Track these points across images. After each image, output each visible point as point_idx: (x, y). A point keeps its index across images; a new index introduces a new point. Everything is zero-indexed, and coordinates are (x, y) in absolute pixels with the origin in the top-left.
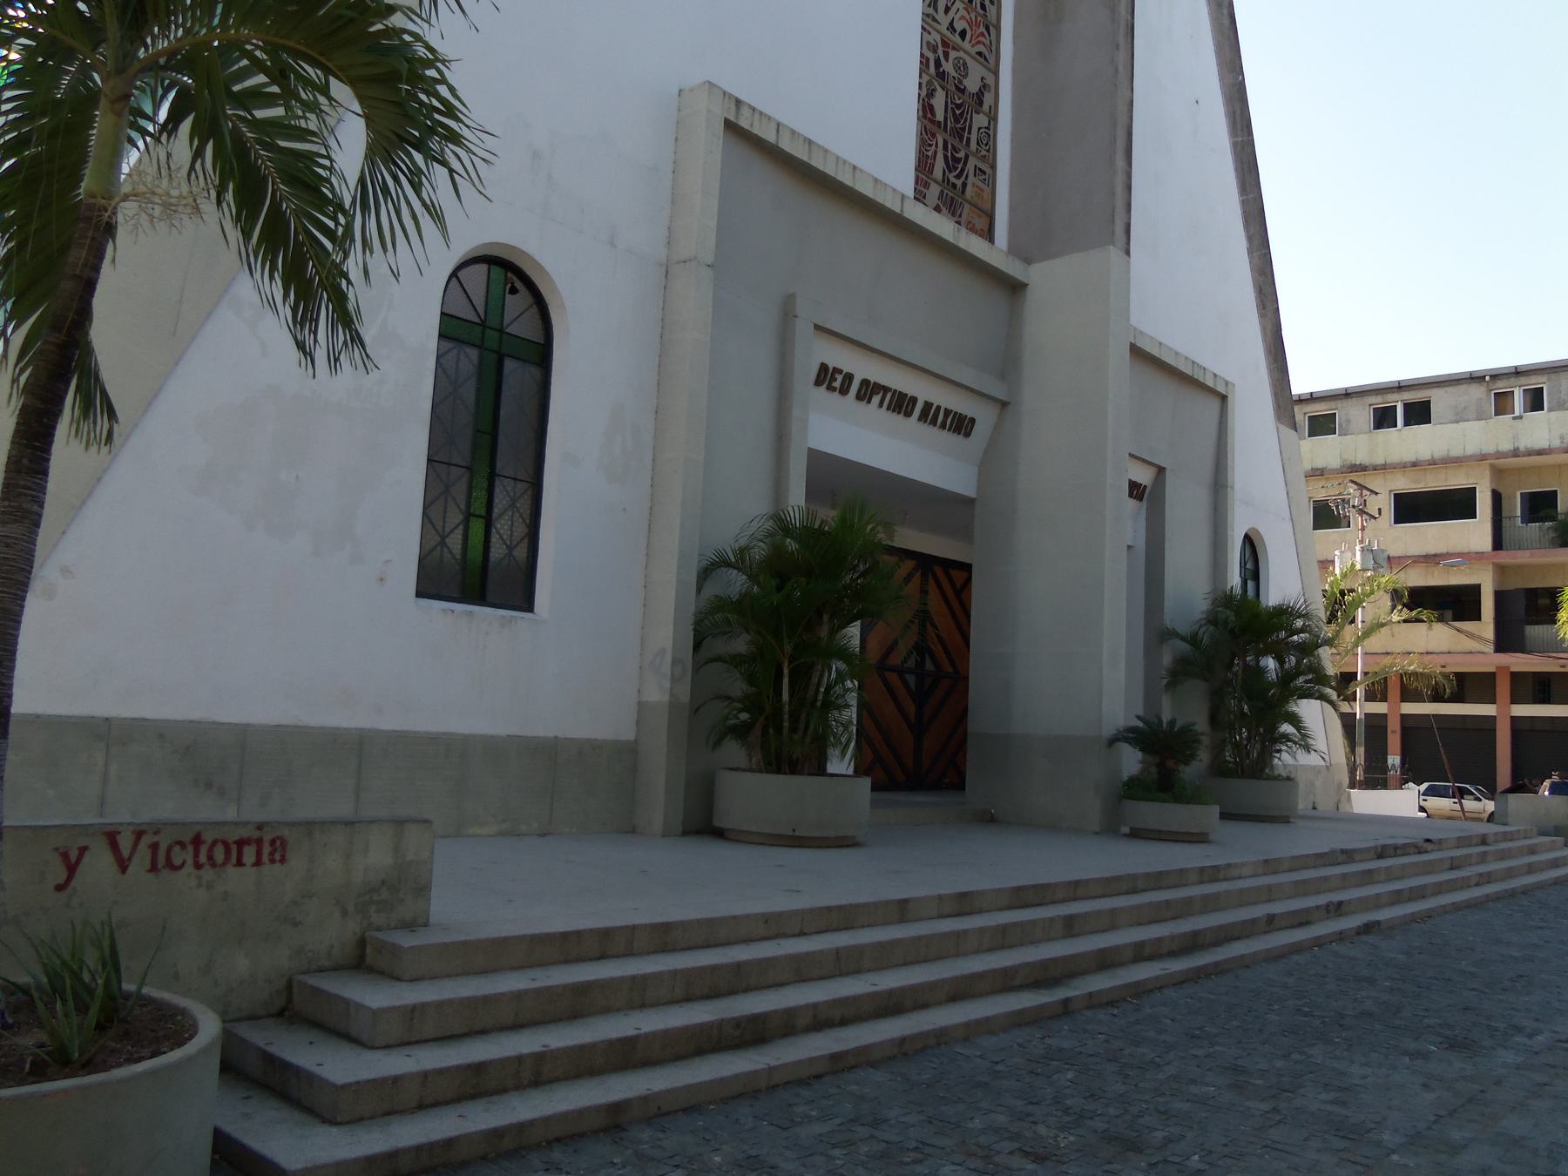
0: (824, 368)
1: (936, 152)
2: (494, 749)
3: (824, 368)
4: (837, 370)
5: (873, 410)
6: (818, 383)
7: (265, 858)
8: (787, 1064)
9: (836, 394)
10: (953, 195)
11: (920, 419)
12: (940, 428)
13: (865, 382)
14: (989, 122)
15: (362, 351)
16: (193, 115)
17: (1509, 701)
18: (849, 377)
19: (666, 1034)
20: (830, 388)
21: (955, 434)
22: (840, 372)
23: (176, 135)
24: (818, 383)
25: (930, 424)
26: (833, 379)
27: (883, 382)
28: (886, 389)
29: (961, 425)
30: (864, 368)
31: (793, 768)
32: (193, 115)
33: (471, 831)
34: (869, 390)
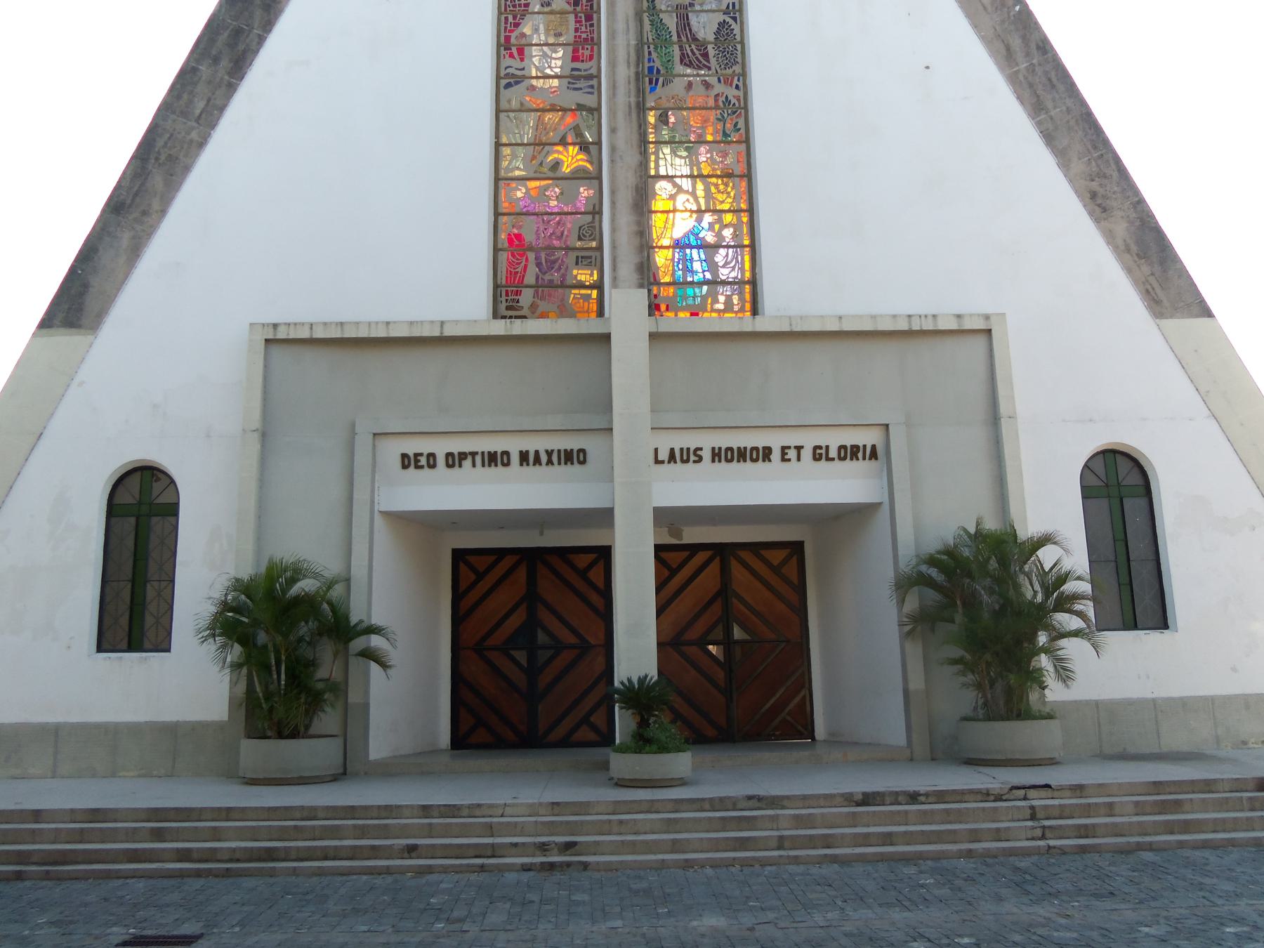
0: (404, 456)
1: (526, 267)
2: (135, 730)
3: (404, 456)
6: (405, 467)
8: (935, 590)
9: (426, 471)
10: (516, 289)
12: (870, 459)
14: (692, 267)
17: (693, 312)
19: (305, 847)
21: (493, 467)
22: (421, 455)
24: (405, 467)
25: (534, 465)
26: (417, 461)
27: (467, 449)
28: (474, 454)
31: (294, 735)
33: (121, 774)
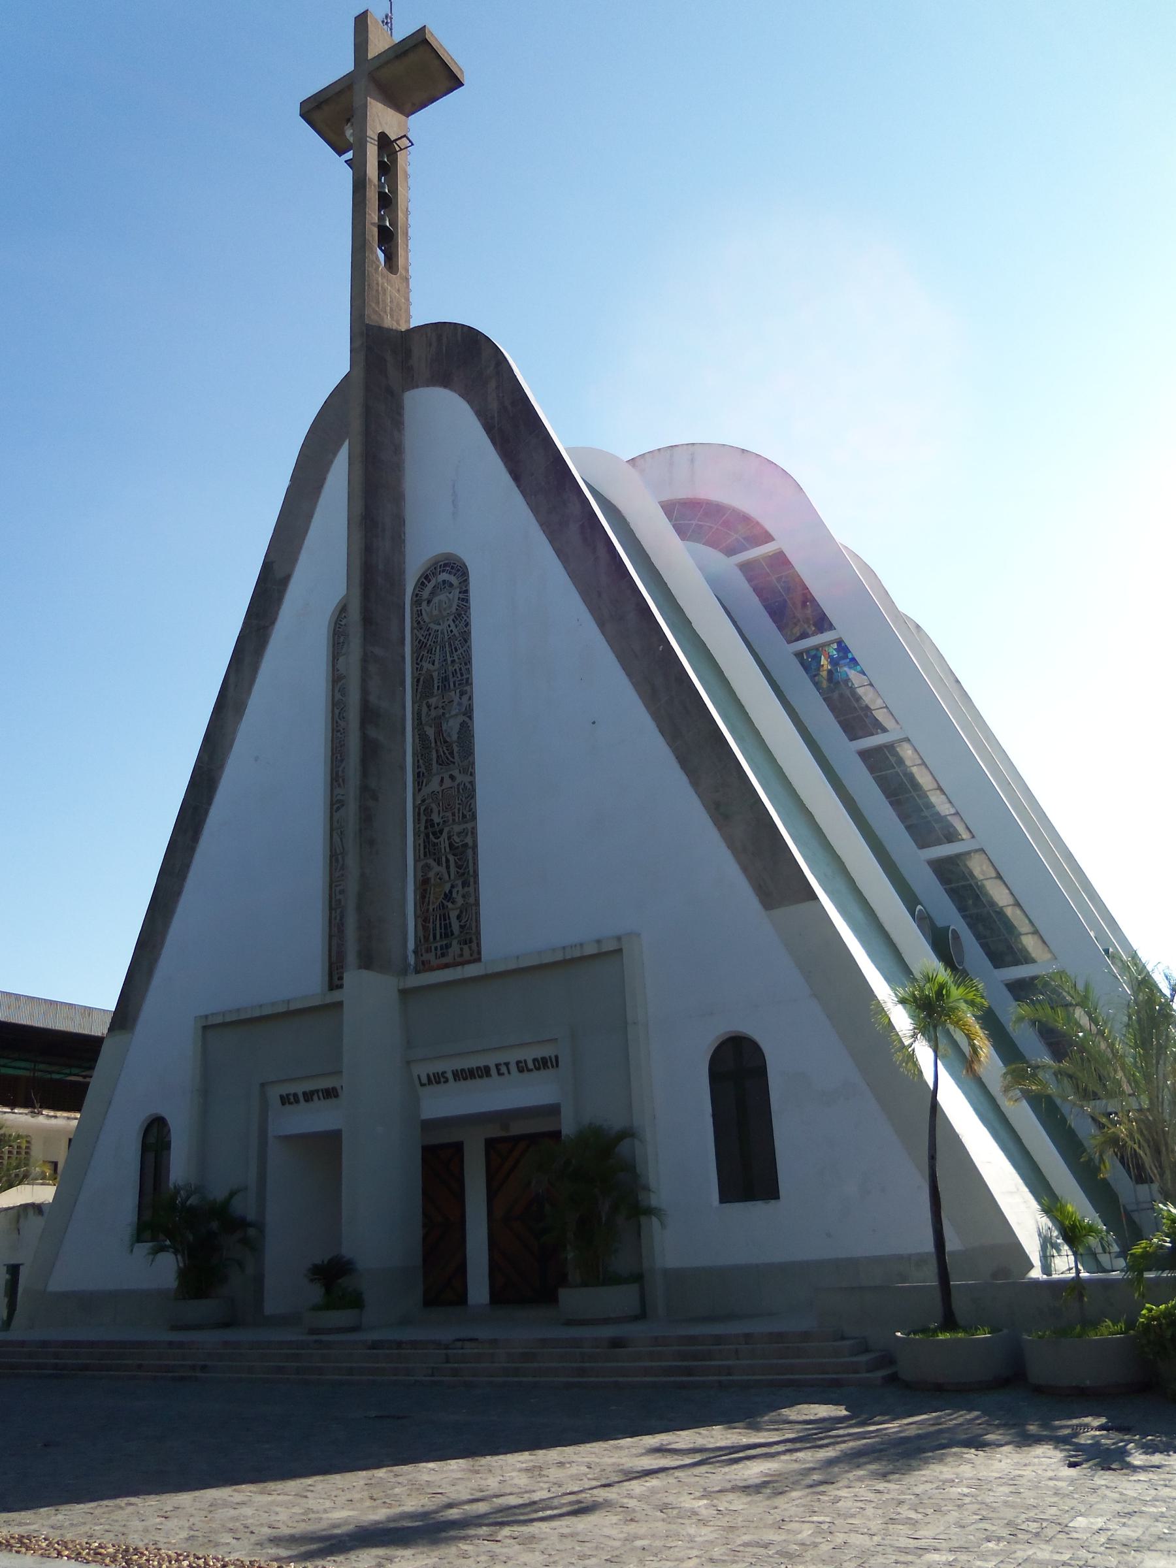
0: (281, 1097)
3: (281, 1097)
4: (288, 1095)
5: (317, 1103)
7: (440, 793)
9: (485, 1078)
11: (455, 1080)
13: (304, 1094)
15: (564, 1510)
16: (347, 443)
18: (295, 1095)
20: (290, 1103)
23: (668, 1444)
24: (283, 1104)
26: (289, 1099)
27: (313, 1088)
28: (317, 1091)
29: (543, 1064)
30: (299, 1088)
32: (347, 443)
34: (308, 1096)
